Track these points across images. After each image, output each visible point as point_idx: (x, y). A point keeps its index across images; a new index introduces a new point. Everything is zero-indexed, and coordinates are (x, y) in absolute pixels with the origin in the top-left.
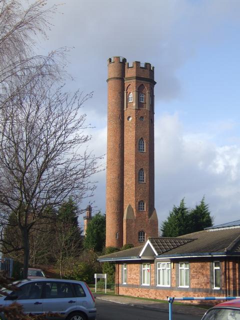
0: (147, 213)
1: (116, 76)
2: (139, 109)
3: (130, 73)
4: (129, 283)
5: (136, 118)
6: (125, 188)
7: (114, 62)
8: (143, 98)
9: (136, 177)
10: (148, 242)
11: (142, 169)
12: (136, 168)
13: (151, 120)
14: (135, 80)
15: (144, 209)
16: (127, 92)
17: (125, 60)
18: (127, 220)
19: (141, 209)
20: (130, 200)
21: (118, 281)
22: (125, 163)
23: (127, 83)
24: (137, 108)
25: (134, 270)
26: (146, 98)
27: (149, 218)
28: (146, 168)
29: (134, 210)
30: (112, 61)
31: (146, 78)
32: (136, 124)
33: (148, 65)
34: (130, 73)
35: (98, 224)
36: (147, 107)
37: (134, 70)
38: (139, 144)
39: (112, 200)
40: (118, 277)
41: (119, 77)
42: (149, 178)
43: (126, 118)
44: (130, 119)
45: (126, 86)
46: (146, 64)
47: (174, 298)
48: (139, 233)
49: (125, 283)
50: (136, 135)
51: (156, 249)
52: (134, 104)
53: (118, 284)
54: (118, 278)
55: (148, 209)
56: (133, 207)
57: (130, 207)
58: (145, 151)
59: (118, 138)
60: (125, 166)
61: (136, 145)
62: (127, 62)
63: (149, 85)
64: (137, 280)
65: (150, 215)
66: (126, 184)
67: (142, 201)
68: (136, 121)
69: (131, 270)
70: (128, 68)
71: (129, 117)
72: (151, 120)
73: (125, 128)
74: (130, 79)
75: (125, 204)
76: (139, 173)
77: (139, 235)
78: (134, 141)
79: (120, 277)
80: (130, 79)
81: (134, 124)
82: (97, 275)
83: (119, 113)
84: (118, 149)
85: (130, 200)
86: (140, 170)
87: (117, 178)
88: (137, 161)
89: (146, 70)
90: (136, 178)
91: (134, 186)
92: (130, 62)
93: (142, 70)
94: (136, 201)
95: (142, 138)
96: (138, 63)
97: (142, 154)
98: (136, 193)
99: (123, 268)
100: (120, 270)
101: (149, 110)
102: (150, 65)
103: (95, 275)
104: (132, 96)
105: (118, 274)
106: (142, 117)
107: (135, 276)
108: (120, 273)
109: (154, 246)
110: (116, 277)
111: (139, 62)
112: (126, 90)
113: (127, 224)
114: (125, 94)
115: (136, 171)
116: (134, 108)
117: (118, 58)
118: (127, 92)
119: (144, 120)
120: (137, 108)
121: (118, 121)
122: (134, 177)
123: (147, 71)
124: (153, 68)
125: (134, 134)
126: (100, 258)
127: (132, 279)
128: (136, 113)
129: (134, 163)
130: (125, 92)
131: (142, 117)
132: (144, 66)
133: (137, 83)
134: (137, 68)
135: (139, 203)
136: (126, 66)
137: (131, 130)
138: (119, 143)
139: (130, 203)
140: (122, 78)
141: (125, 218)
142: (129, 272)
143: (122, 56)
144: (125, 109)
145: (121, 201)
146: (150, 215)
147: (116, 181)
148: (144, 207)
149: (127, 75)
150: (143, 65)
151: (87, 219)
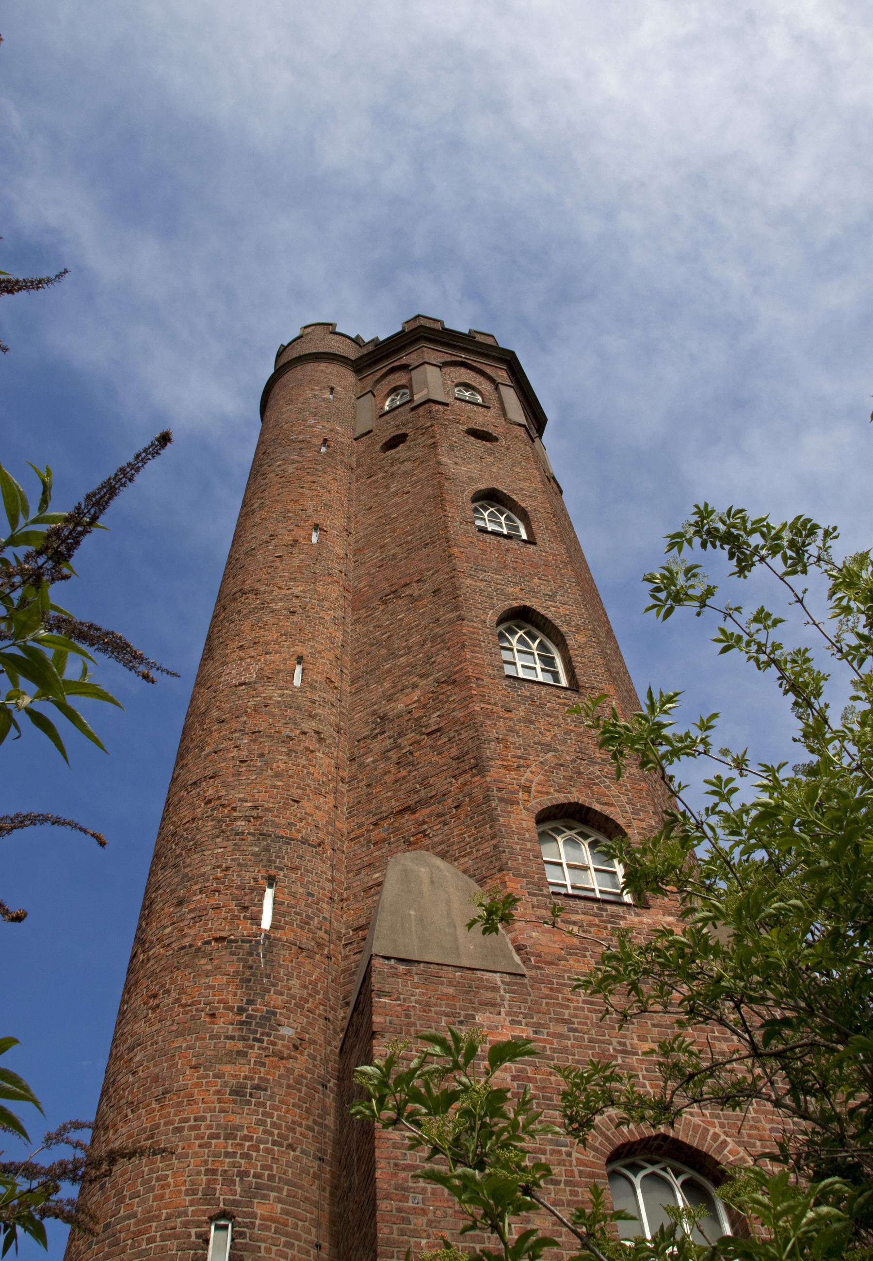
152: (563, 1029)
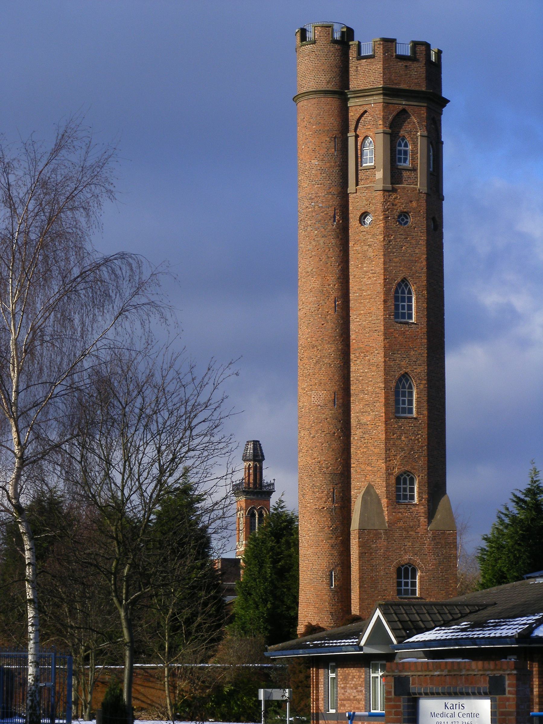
0: (422, 509)
1: (324, 87)
2: (394, 190)
3: (367, 75)
4: (342, 710)
5: (386, 218)
6: (356, 434)
7: (314, 42)
8: (406, 152)
9: (387, 398)
10: (378, 613)
11: (405, 377)
12: (386, 373)
13: (434, 219)
14: (380, 99)
15: (412, 497)
16: (357, 136)
17: (348, 34)
18: (361, 531)
19: (405, 497)
20: (370, 472)
21: (317, 707)
22: (352, 356)
23: (355, 106)
24: (389, 186)
25: (354, 677)
26: (414, 153)
27: (429, 522)
28: (419, 370)
29: (384, 501)
30: (310, 35)
31: (418, 89)
32: (386, 235)
33: (421, 47)
34: (367, 75)
35: (276, 537)
36: (420, 183)
37: (377, 66)
38: (396, 299)
39: (317, 471)
40: (317, 696)
41: (330, 87)
42: (428, 401)
43: (353, 222)
44: (368, 220)
45: (353, 115)
46: (415, 44)
47: (354, 713)
48: (399, 570)
49: (332, 711)
50: (385, 269)
51: (393, 630)
52: (379, 175)
53: (317, 714)
54: (317, 700)
55: (425, 496)
56: (381, 490)
57: (369, 491)
58: (413, 320)
59: (332, 279)
60: (353, 368)
61: (385, 301)
62: (357, 37)
63: (424, 113)
64: (359, 701)
65: (431, 514)
66: (359, 423)
67: (407, 472)
68: (386, 228)
69: (345, 679)
70: (360, 57)
71: (364, 215)
72: (434, 219)
73: (354, 248)
74: (363, 93)
75: (354, 483)
76: (397, 387)
77: (399, 576)
78: (380, 288)
79: (321, 697)
80: (363, 93)
81: (381, 237)
82: (265, 693)
83: (335, 202)
84: (332, 315)
85: (370, 472)
86: (400, 380)
87: (330, 405)
88: (390, 350)
89: (415, 65)
90: (387, 405)
91: (382, 427)
92: (367, 41)
93: (401, 64)
94: (389, 474)
95: (404, 280)
96: (389, 43)
97: (403, 328)
98: (387, 449)
99: (326, 677)
100: (321, 679)
101: (425, 190)
102: (427, 46)
103: (261, 692)
104: (372, 153)
105: (317, 690)
106: (403, 216)
107: (354, 693)
108: (321, 687)
109: (388, 622)
110: (313, 696)
111: (393, 41)
112: (352, 127)
113: (361, 545)
114: (351, 141)
115: (386, 382)
116: (380, 186)
117: (328, 27)
118: (357, 136)
119: (411, 220)
120: (389, 186)
121: (332, 226)
122: (382, 400)
123: (418, 71)
124: (439, 53)
125: (380, 269)
126: (271, 650)
127: (349, 699)
128: (385, 202)
129: (380, 359)
130: (351, 134)
131: (403, 216)
132: (408, 53)
133: (386, 105)
134: (386, 60)
135: (398, 480)
136: (353, 53)
137: (370, 254)
138: (334, 294)
139: (370, 478)
140: (340, 92)
141: (355, 525)
142: (341, 684)
143: (341, 19)
144: (351, 188)
145: (342, 474)
146: (431, 514)
147: (328, 413)
148: (412, 490)
149: (354, 84)
150: (405, 50)
151: (246, 492)
152: (393, 542)
